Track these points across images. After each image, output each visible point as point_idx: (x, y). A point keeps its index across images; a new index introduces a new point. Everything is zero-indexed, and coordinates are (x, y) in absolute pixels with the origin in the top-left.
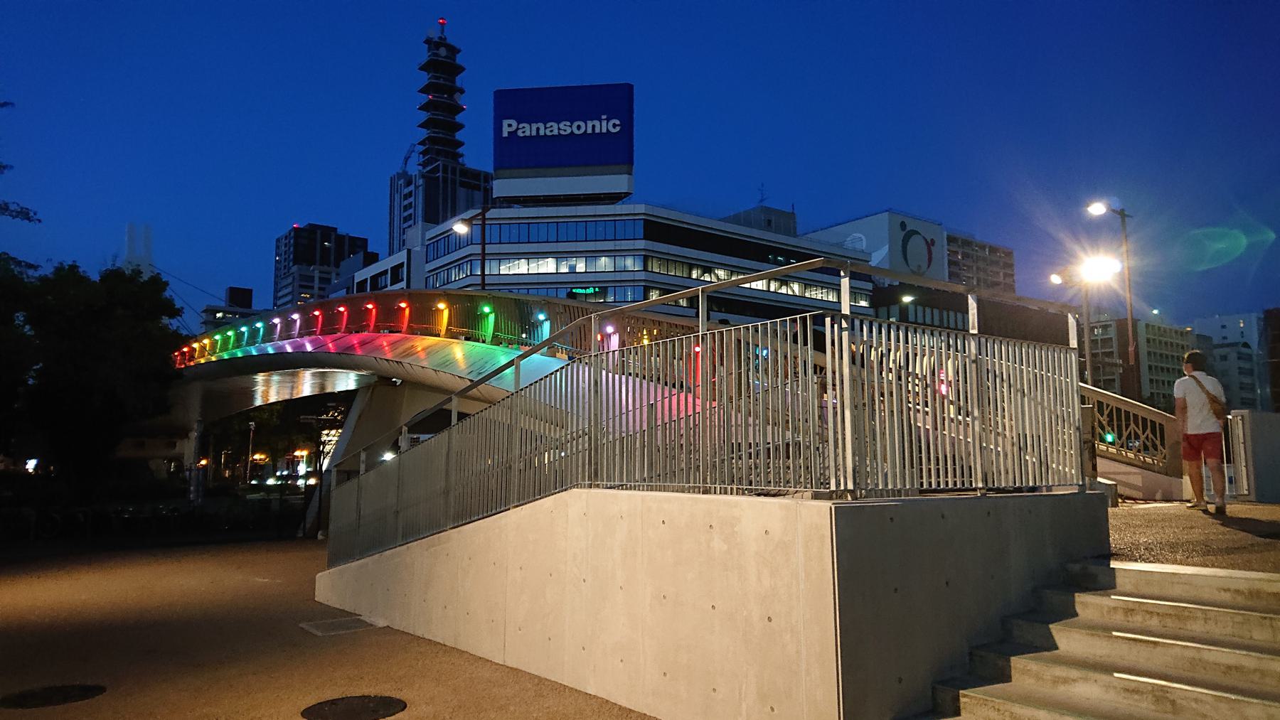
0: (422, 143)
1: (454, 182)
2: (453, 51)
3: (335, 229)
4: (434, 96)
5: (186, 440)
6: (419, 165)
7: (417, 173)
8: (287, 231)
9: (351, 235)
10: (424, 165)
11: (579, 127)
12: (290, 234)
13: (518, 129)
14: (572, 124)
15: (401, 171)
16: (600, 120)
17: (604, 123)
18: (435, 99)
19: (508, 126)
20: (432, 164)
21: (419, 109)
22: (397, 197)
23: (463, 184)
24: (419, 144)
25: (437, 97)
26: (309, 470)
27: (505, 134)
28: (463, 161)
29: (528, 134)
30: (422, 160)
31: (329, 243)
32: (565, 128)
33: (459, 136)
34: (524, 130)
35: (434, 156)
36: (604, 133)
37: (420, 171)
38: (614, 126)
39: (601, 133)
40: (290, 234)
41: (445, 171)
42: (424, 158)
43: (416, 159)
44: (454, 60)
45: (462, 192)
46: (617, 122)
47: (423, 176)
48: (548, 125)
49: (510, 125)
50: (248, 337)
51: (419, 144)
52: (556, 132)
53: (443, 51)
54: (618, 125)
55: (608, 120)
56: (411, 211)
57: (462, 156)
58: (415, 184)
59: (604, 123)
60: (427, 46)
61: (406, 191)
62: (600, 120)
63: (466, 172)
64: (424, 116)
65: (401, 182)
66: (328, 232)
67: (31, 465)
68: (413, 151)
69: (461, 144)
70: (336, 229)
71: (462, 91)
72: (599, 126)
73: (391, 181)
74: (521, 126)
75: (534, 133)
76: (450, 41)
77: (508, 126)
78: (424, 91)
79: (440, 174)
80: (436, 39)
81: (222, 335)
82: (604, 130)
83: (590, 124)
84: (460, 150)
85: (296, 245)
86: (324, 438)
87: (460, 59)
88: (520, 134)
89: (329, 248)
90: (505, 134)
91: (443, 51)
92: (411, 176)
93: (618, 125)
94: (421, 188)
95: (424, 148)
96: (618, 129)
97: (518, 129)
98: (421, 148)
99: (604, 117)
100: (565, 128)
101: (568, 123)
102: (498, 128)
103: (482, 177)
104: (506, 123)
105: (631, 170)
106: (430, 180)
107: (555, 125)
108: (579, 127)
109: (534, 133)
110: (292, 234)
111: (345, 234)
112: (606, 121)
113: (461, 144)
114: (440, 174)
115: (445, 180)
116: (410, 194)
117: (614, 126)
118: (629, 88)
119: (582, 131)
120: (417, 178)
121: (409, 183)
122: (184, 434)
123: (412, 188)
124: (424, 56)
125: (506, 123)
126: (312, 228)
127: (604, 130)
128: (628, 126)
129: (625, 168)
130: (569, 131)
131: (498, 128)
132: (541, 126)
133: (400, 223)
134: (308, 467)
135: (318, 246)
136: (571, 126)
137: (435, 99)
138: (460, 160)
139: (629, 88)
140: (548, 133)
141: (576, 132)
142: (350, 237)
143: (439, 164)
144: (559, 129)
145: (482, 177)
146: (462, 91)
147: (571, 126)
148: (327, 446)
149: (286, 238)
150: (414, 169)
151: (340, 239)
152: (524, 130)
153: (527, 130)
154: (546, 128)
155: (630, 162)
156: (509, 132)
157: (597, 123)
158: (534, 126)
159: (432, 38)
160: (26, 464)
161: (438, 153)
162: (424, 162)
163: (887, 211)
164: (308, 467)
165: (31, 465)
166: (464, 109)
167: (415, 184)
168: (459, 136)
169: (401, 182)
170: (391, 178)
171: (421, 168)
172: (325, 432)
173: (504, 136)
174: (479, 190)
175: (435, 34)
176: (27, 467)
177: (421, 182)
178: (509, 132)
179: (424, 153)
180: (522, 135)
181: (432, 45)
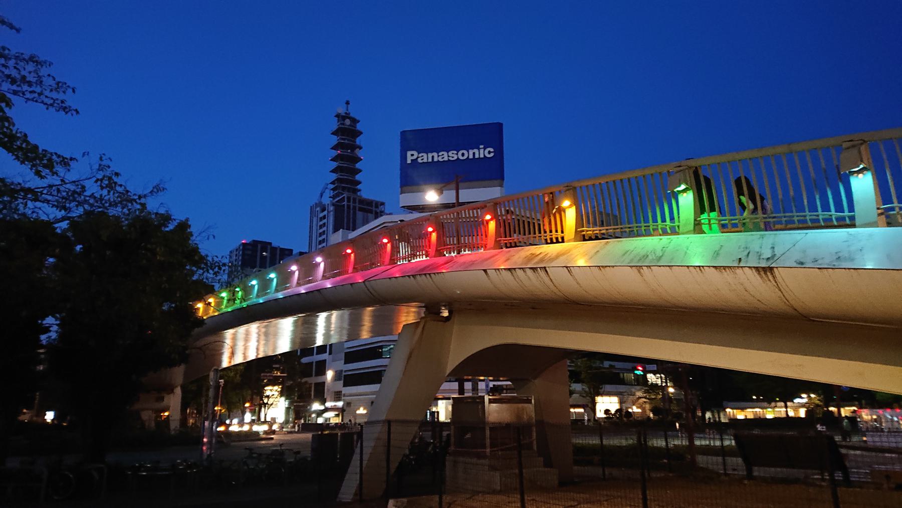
0: (333, 183)
1: (354, 208)
2: (355, 121)
3: (270, 244)
4: (341, 152)
5: (171, 395)
6: (330, 197)
7: (329, 202)
8: (238, 245)
9: (281, 247)
10: (333, 197)
11: (463, 155)
12: (239, 248)
13: (418, 157)
14: (458, 152)
15: (317, 202)
16: (479, 149)
17: (482, 151)
18: (342, 153)
19: (411, 156)
20: (339, 197)
21: (331, 160)
22: (315, 219)
23: (361, 210)
24: (330, 183)
25: (343, 152)
26: (253, 418)
27: (409, 162)
28: (360, 194)
29: (425, 160)
30: (332, 194)
31: (266, 253)
32: (453, 155)
33: (358, 177)
34: (422, 158)
35: (340, 191)
36: (482, 158)
37: (331, 201)
38: (489, 152)
39: (479, 158)
40: (239, 248)
41: (349, 201)
42: (333, 192)
43: (328, 193)
44: (356, 128)
45: (360, 215)
46: (492, 150)
47: (333, 205)
48: (440, 154)
49: (412, 155)
50: (258, 290)
51: (330, 183)
52: (446, 159)
53: (348, 122)
54: (492, 152)
55: (485, 149)
56: (325, 229)
57: (360, 190)
58: (328, 210)
59: (482, 151)
60: (337, 118)
61: (322, 215)
62: (479, 149)
63: (363, 201)
64: (335, 165)
65: (318, 209)
66: (265, 245)
67: (50, 416)
68: (327, 188)
69: (359, 183)
70: (271, 243)
71: (360, 148)
72: (478, 153)
73: (311, 209)
74: (420, 155)
75: (430, 160)
76: (352, 115)
77: (411, 156)
78: (335, 148)
79: (345, 203)
80: (344, 115)
81: (216, 298)
82: (482, 156)
83: (471, 152)
84: (359, 187)
85: (243, 255)
86: (268, 393)
87: (359, 127)
88: (420, 160)
89: (266, 257)
90: (409, 162)
91: (348, 122)
92: (325, 205)
93: (492, 152)
94: (332, 213)
95: (334, 186)
96: (492, 155)
97: (418, 157)
98: (332, 186)
99: (482, 146)
100: (453, 155)
101: (456, 152)
102: (404, 157)
103: (374, 205)
104: (409, 153)
105: (503, 184)
106: (338, 208)
107: (445, 154)
108: (463, 155)
109: (430, 160)
110: (241, 248)
111: (277, 247)
112: (483, 150)
113: (359, 183)
114: (345, 203)
115: (349, 207)
116: (324, 217)
117: (489, 152)
118: (500, 125)
119: (465, 157)
120: (329, 206)
121: (323, 210)
122: (170, 390)
123: (325, 213)
124: (335, 125)
125: (409, 153)
126: (255, 243)
127: (482, 156)
128: (499, 152)
129: (498, 182)
130: (456, 157)
131: (404, 157)
132: (435, 154)
133: (327, 230)
134: (252, 416)
135: (259, 254)
136: (457, 154)
137: (342, 153)
138: (359, 193)
139: (500, 125)
140: (441, 160)
141: (461, 158)
142: (280, 248)
143: (344, 197)
144: (448, 156)
145: (374, 205)
146: (360, 148)
147: (457, 154)
148: (270, 399)
149: (237, 250)
150: (327, 200)
151: (274, 249)
152: (422, 158)
153: (425, 158)
154: (438, 156)
155: (502, 178)
156: (412, 160)
157: (476, 151)
158: (430, 155)
159: (340, 114)
160: (45, 415)
161: (344, 189)
162: (333, 195)
163: (537, 255)
164: (252, 416)
165: (50, 416)
166: (361, 159)
167: (328, 210)
168: (358, 177)
169: (318, 209)
170: (311, 207)
171: (332, 199)
172: (270, 388)
173: (408, 162)
174: (372, 213)
175: (342, 110)
176: (46, 417)
177: (332, 208)
178: (412, 160)
179: (333, 189)
180: (421, 161)
181: (340, 119)
